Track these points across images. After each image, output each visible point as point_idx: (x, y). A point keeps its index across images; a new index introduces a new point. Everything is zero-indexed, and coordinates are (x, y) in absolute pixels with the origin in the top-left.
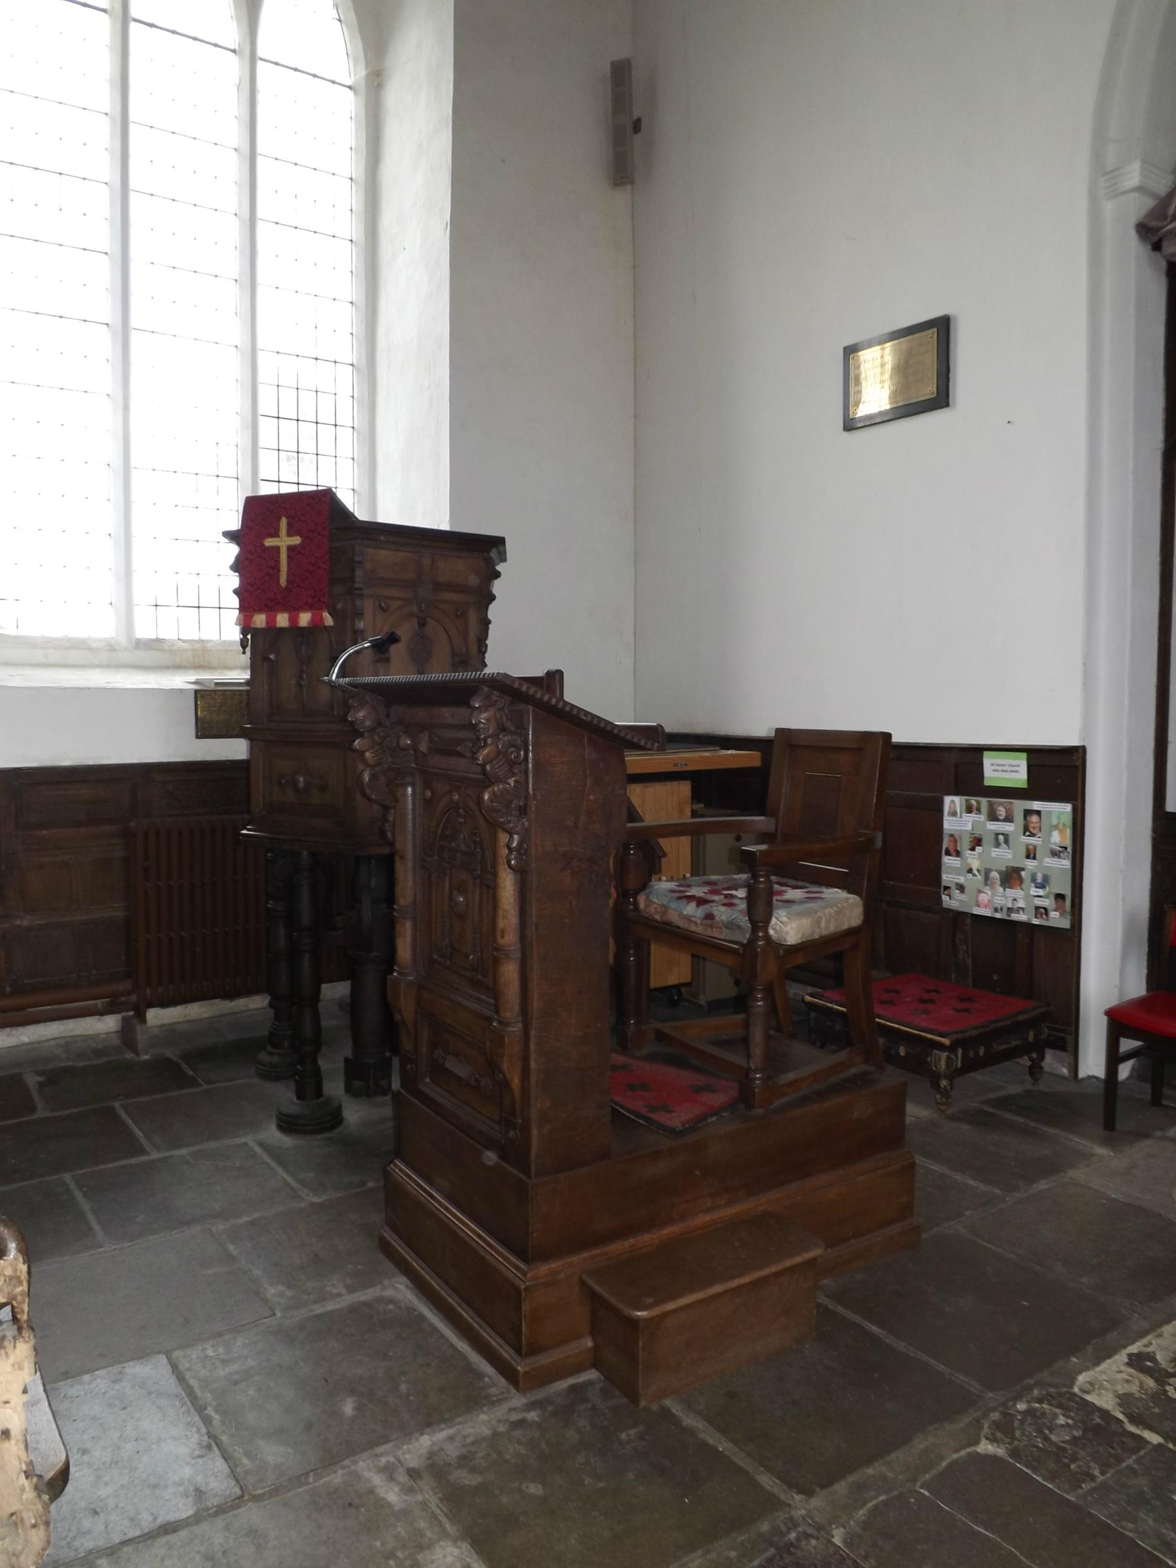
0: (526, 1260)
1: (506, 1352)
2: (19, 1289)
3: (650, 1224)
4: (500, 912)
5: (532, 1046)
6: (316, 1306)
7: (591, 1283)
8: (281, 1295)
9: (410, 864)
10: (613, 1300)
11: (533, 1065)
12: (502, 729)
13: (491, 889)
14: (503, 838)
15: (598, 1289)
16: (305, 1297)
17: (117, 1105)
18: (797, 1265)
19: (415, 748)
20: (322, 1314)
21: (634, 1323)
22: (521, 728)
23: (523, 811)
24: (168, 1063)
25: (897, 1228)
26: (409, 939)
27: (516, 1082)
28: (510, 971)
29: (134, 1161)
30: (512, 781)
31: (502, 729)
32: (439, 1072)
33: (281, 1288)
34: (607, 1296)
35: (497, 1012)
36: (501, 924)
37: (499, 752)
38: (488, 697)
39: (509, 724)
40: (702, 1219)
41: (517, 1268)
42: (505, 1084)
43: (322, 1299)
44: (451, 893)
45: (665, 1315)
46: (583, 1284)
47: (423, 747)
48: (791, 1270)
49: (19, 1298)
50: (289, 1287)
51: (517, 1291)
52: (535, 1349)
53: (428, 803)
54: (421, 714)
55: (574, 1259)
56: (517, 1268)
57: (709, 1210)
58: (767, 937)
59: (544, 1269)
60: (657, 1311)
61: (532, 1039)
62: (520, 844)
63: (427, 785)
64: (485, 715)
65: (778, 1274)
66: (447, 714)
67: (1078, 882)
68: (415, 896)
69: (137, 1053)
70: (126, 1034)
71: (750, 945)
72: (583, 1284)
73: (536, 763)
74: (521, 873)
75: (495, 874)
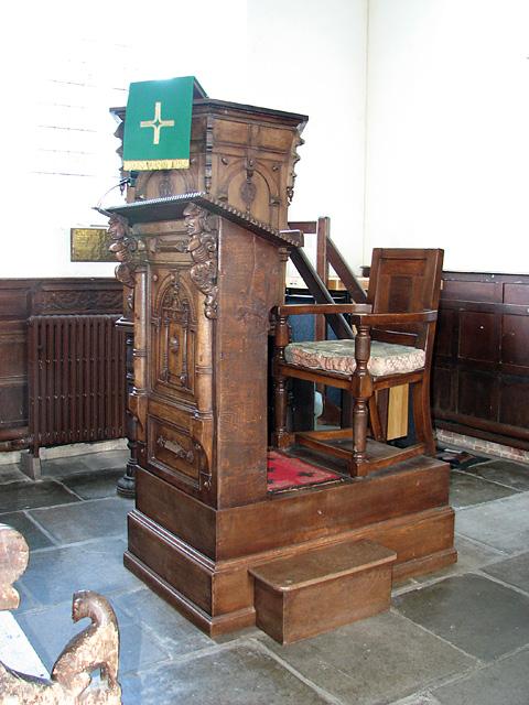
0: (214, 560)
1: (202, 615)
2: (112, 652)
3: (291, 542)
4: (200, 345)
5: (219, 428)
6: (196, 652)
7: (255, 573)
8: (169, 644)
9: (143, 323)
10: (267, 582)
11: (219, 439)
12: (203, 230)
13: (193, 332)
14: (202, 298)
15: (258, 576)
16: (187, 646)
17: (25, 512)
18: (378, 566)
19: (147, 249)
20: (203, 658)
21: (280, 595)
22: (215, 230)
23: (215, 282)
24: (54, 484)
25: (443, 553)
26: (143, 370)
27: (209, 451)
28: (205, 382)
29: (46, 550)
30: (208, 263)
31: (203, 230)
32: (161, 451)
33: (168, 639)
34: (263, 579)
35: (197, 407)
36: (200, 353)
37: (201, 244)
38: (194, 210)
39: (206, 227)
40: (322, 541)
41: (208, 564)
42: (202, 452)
43: (199, 648)
44: (169, 340)
45: (299, 590)
46: (249, 574)
47: (152, 248)
48: (377, 568)
49: (112, 659)
50: (174, 639)
51: (210, 577)
52: (219, 613)
53: (155, 283)
54: (152, 228)
55: (244, 560)
56: (208, 564)
57: (326, 536)
58: (367, 371)
59: (225, 565)
60: (295, 587)
61: (219, 423)
62: (213, 302)
63: (155, 272)
64: (193, 221)
65: (369, 570)
66: (168, 226)
67: (512, 441)
68: (146, 342)
69: (33, 479)
70: (25, 466)
71: (355, 375)
72: (249, 574)
73: (223, 252)
74: (213, 320)
75: (197, 323)
